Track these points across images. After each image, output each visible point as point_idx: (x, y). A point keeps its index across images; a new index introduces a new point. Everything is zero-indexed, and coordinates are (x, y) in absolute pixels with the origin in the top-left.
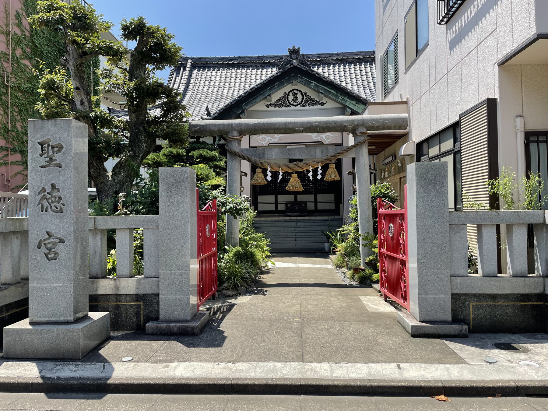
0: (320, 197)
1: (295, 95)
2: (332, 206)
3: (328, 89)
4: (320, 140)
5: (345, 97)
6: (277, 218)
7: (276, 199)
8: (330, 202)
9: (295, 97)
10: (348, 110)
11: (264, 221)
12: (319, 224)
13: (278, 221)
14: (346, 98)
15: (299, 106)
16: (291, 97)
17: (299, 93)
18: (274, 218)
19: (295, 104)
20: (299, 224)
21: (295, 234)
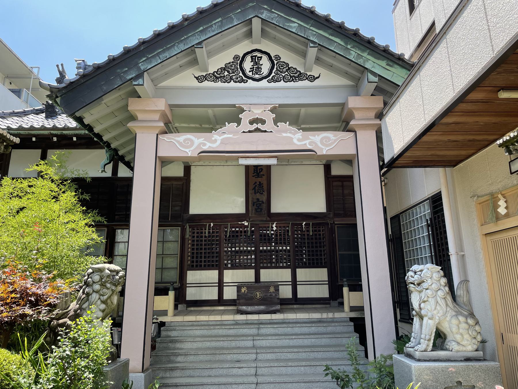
0: (302, 274)
1: (256, 61)
2: (323, 292)
3: (327, 35)
4: (310, 147)
5: (363, 51)
6: (218, 318)
7: (295, 291)
8: (318, 283)
9: (256, 63)
10: (372, 78)
11: (193, 324)
12: (306, 330)
13: (222, 324)
14: (365, 55)
15: (265, 81)
16: (248, 65)
17: (265, 58)
18: (212, 318)
19: (257, 76)
20: (263, 331)
21: (254, 356)
